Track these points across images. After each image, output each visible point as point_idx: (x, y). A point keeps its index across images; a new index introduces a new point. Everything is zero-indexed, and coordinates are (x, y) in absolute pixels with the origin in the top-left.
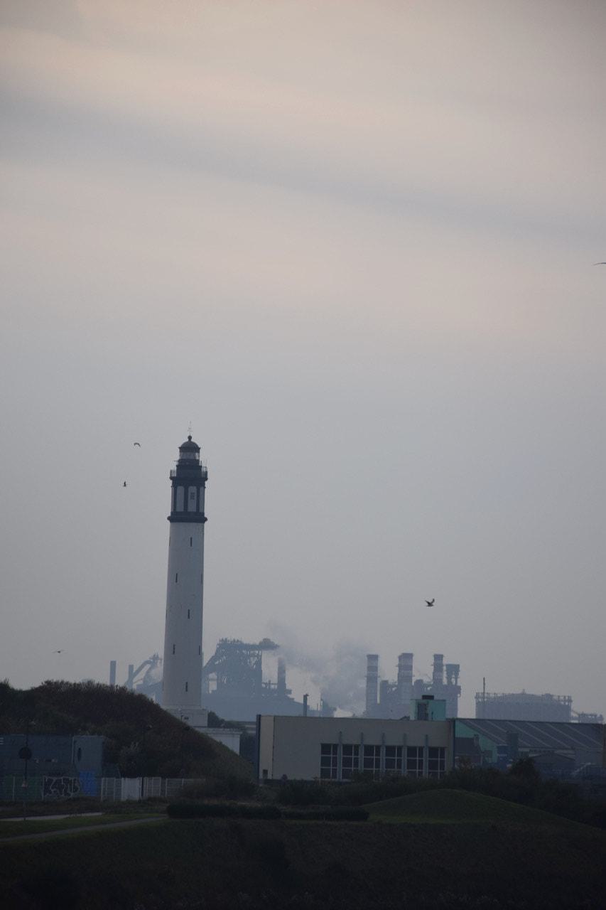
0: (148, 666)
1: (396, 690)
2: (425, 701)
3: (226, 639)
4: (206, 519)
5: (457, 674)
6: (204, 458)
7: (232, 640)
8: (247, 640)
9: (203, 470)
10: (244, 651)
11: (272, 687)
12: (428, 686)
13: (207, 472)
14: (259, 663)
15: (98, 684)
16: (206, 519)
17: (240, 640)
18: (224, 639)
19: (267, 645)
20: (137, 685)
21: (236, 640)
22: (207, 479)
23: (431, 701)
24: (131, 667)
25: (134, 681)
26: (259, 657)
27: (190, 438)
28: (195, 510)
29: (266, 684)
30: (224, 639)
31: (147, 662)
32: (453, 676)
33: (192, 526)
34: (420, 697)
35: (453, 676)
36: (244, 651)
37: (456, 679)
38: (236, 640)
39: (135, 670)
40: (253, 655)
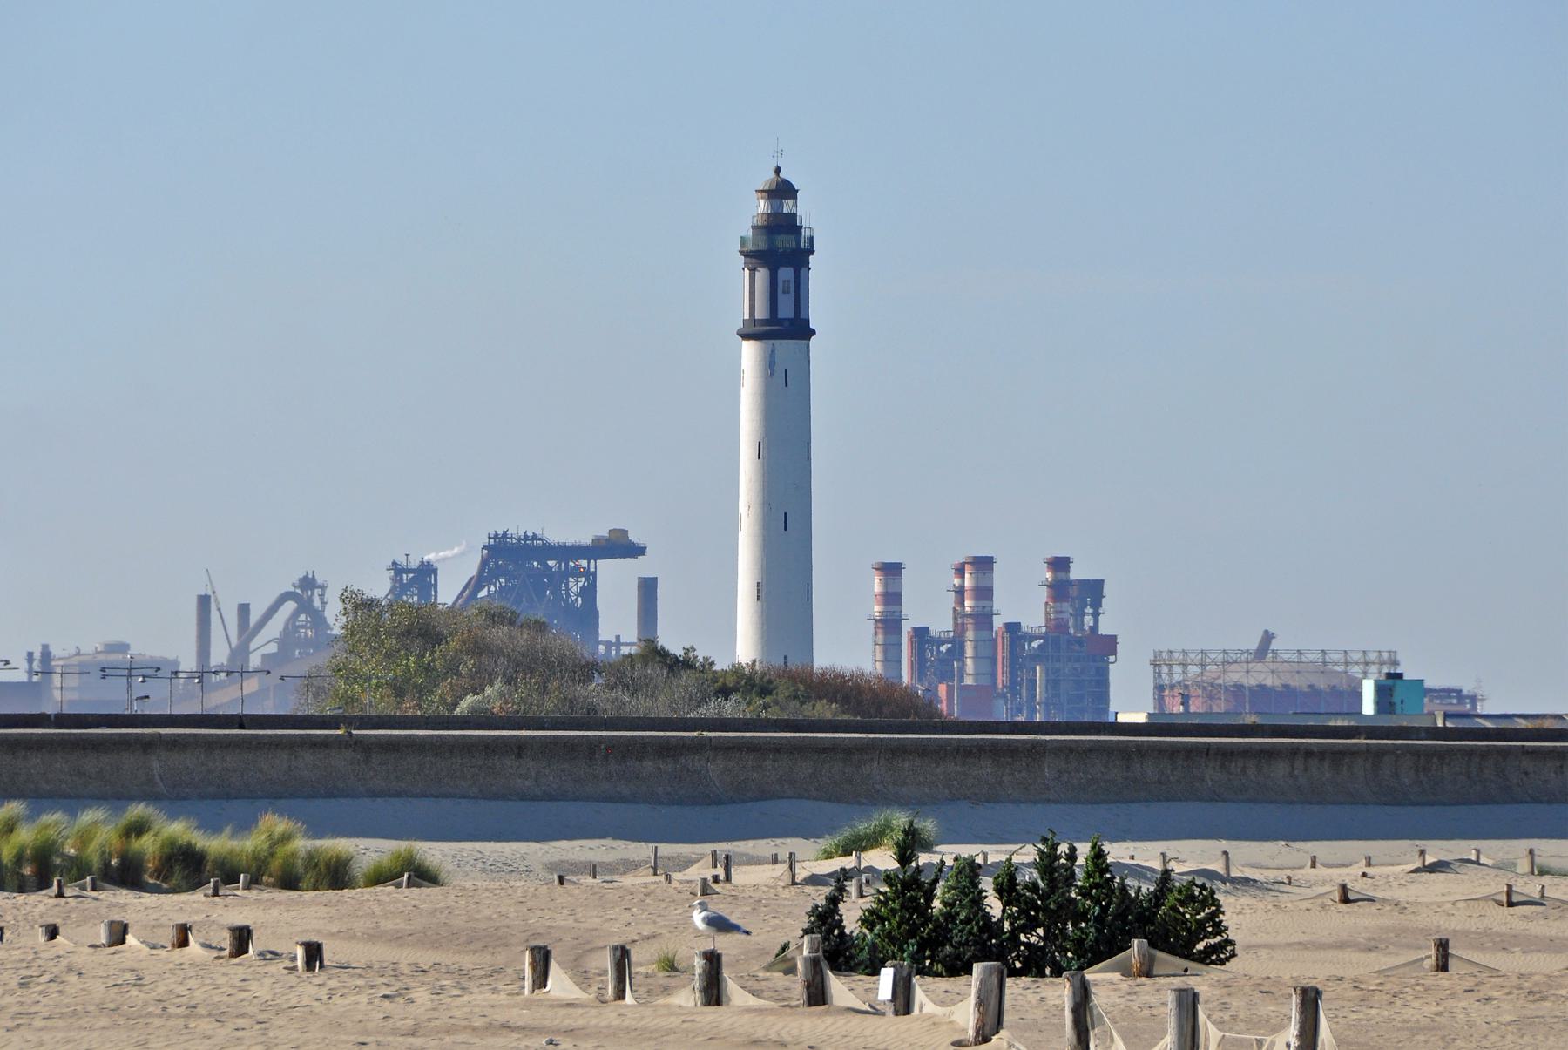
0: (290, 606)
1: (948, 650)
2: (1390, 682)
3: (505, 534)
4: (813, 332)
5: (1097, 604)
6: (806, 210)
7: (521, 534)
8: (558, 534)
9: (805, 233)
10: (551, 563)
11: (625, 650)
12: (1036, 638)
13: (811, 239)
14: (589, 592)
15: (823, 674)
16: (813, 332)
17: (538, 533)
18: (500, 533)
19: (619, 546)
20: (264, 656)
21: (530, 534)
22: (812, 252)
23: (1399, 682)
24: (244, 610)
25: (253, 646)
26: (591, 576)
27: (778, 170)
28: (791, 315)
29: (608, 644)
30: (500, 533)
31: (285, 597)
32: (1089, 610)
33: (785, 346)
34: (1383, 677)
35: (1089, 610)
36: (551, 563)
37: (1096, 615)
38: (530, 534)
39: (254, 617)
40: (577, 573)
